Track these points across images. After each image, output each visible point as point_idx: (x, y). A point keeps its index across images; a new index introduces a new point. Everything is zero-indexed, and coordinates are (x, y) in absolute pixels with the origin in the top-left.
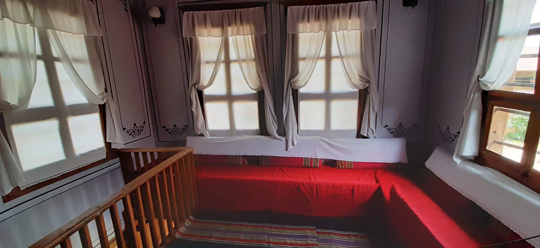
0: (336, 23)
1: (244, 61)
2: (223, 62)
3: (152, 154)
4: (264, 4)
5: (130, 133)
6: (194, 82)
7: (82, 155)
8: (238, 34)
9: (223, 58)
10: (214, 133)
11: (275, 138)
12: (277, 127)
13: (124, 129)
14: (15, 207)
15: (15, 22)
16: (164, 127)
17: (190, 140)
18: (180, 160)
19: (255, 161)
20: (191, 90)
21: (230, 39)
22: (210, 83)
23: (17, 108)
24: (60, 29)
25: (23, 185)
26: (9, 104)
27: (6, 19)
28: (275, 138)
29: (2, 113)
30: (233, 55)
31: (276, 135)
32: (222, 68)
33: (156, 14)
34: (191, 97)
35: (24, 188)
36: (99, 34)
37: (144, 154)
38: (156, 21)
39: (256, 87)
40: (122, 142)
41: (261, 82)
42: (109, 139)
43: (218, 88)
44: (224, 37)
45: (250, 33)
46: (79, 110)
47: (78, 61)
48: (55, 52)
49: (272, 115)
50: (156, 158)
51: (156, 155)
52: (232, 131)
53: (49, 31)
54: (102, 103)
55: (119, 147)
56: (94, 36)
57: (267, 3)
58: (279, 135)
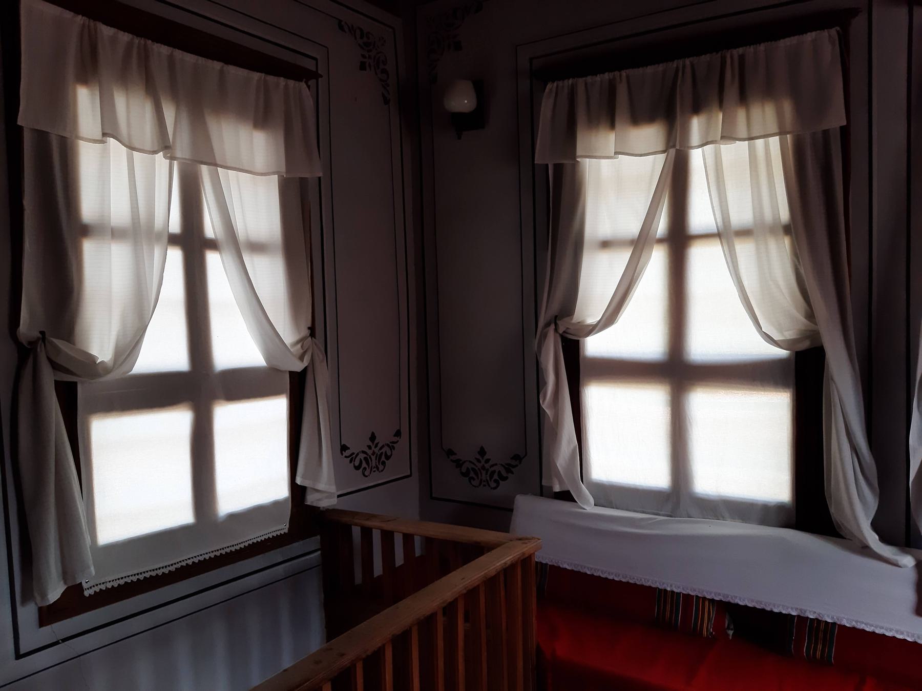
0: (779, 256)
1: (745, 233)
2: (660, 241)
3: (408, 539)
4: (837, 19)
5: (357, 463)
6: (555, 307)
7: (234, 517)
8: (728, 136)
9: (662, 226)
10: (609, 494)
11: (865, 550)
12: (873, 503)
13: (344, 448)
14: (64, 640)
15: (131, 148)
16: (450, 452)
17: (530, 511)
18: (491, 582)
19: (765, 633)
20: (544, 336)
21: (697, 158)
22: (610, 318)
23: (105, 369)
24: (229, 165)
25: (92, 579)
26: (92, 358)
27: (112, 141)
28: (865, 550)
29: (75, 384)
30: (701, 214)
31: (872, 539)
32: (657, 262)
33: (462, 101)
34: (542, 359)
35: (91, 592)
36: (314, 171)
37: (388, 536)
38: (464, 123)
39: (789, 335)
40: (333, 489)
41: (810, 315)
42: (303, 477)
43: (636, 333)
44: (672, 152)
45: (774, 128)
46: (243, 385)
47: (257, 248)
48: (211, 227)
49: (855, 449)
50: (418, 553)
51: (417, 541)
52: (678, 497)
53: (205, 170)
54: (298, 367)
55: (325, 503)
56: (301, 179)
57: (853, 12)
58: (885, 539)
